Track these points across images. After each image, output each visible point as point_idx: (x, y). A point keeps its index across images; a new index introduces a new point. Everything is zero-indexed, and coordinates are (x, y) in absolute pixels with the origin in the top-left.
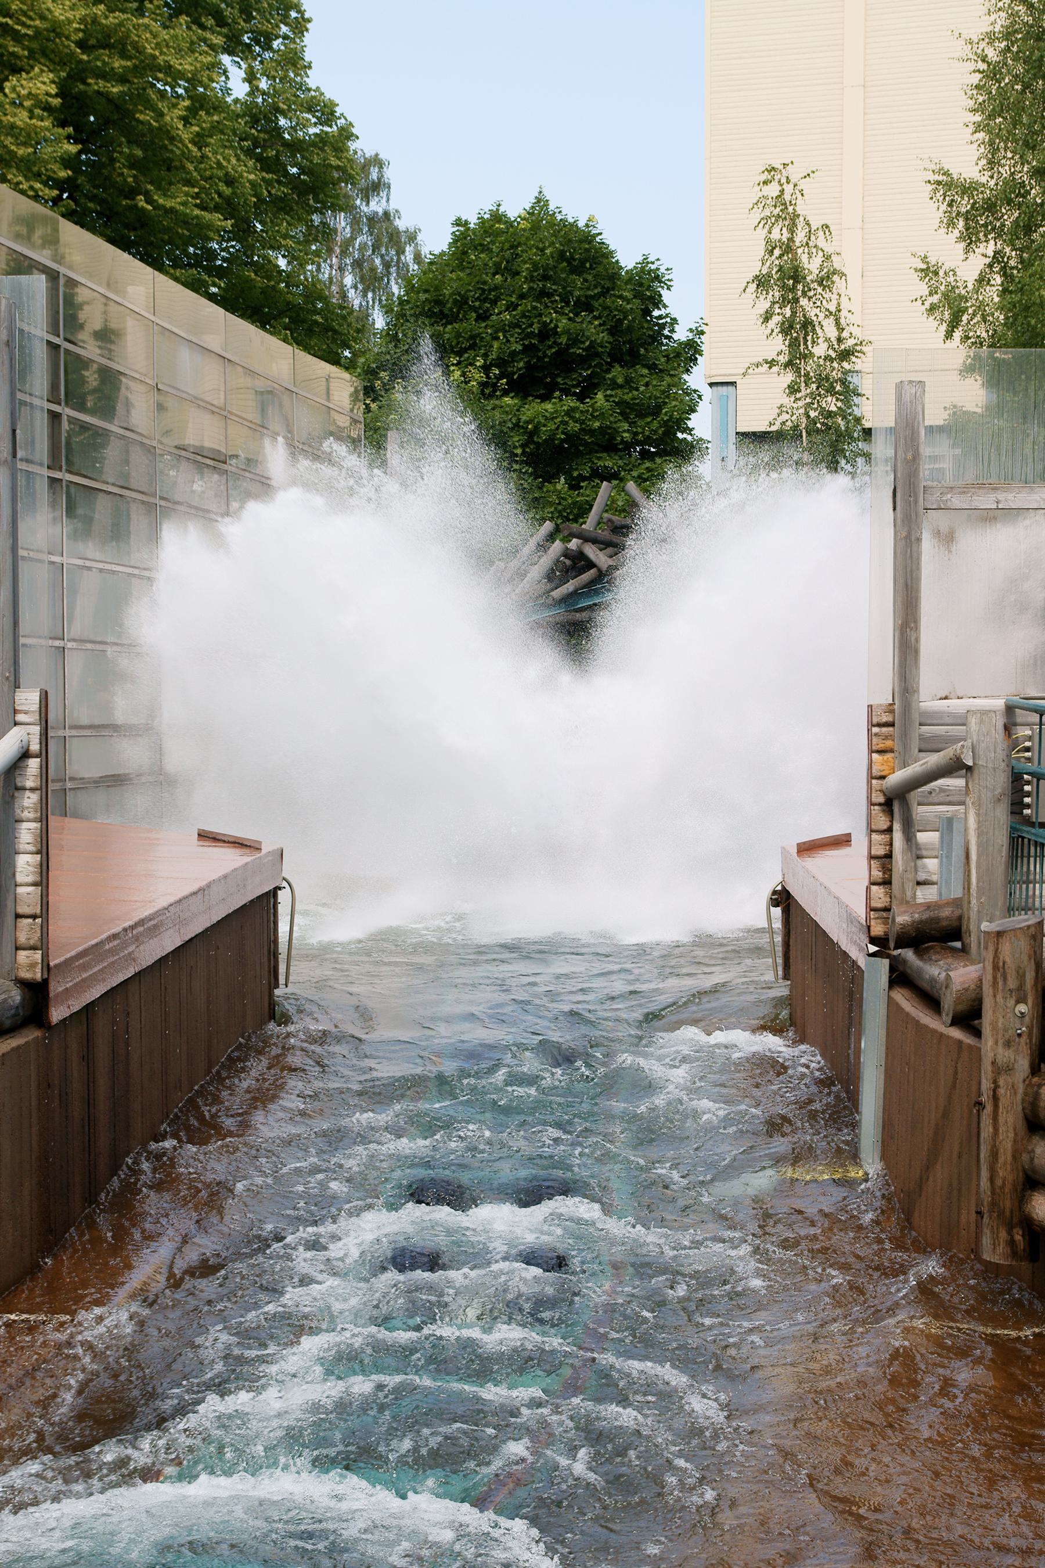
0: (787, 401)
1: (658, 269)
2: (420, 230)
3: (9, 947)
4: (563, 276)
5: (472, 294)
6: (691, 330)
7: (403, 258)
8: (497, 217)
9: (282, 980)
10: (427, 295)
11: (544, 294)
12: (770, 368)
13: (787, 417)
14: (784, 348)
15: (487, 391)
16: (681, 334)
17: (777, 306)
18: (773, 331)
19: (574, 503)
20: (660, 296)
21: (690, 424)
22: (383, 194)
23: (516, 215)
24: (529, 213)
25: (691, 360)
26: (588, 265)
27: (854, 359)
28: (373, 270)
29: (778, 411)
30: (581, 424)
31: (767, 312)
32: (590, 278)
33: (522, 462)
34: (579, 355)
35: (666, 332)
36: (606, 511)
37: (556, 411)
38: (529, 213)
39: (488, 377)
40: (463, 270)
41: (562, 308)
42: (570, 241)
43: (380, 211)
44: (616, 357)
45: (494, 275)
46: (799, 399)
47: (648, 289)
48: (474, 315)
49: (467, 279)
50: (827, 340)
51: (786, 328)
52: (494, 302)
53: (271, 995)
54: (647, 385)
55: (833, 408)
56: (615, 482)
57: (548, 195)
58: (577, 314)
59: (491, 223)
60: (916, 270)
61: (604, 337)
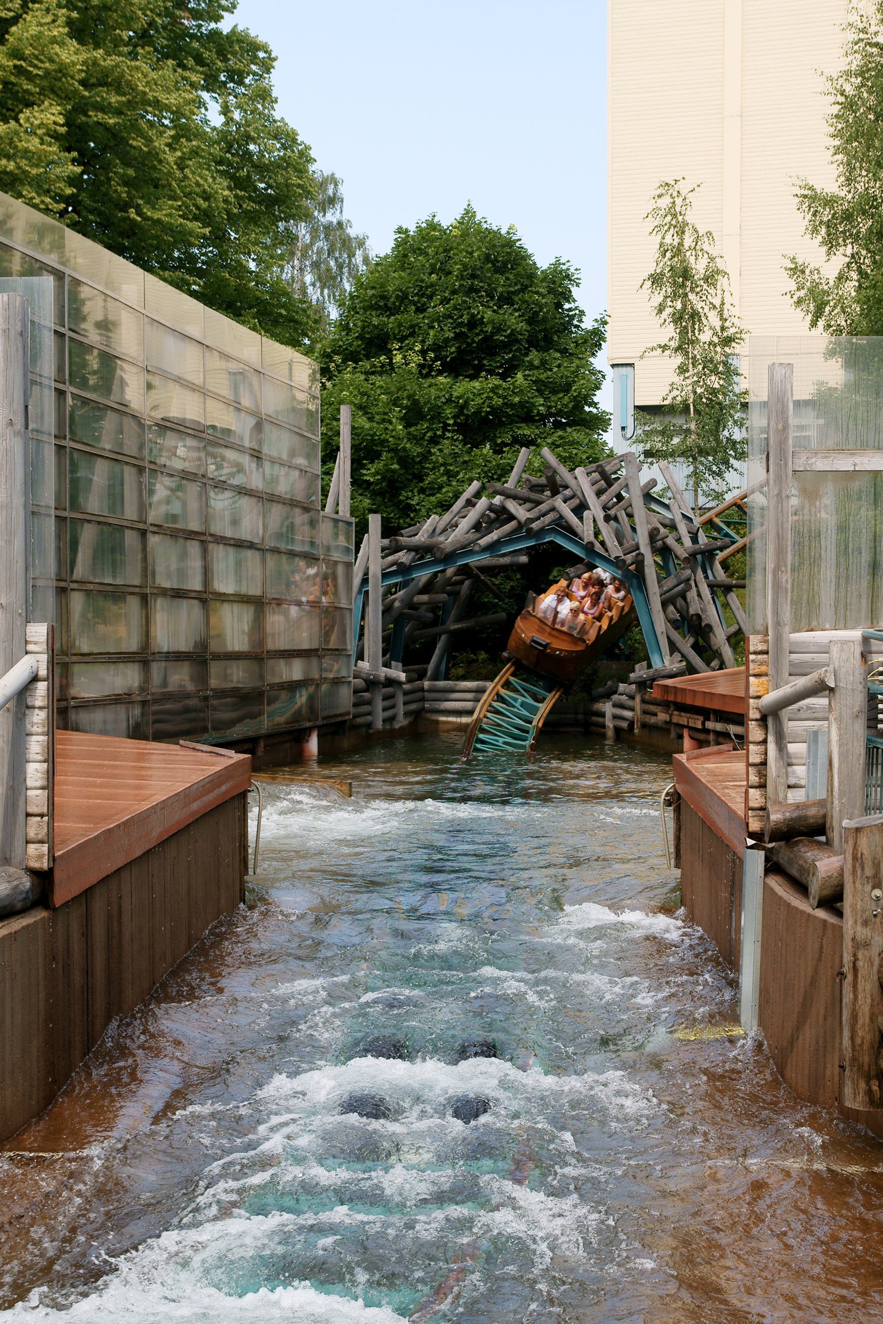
0: (678, 379)
6: (596, 320)
8: (433, 226)
10: (373, 292)
11: (472, 290)
13: (678, 393)
14: (674, 335)
15: (424, 372)
16: (588, 324)
17: (669, 300)
19: (498, 465)
20: (570, 291)
21: (595, 399)
22: (338, 206)
27: (734, 344)
28: (329, 270)
32: (511, 277)
33: (453, 431)
35: (575, 322)
36: (524, 471)
39: (425, 360)
42: (494, 246)
43: (335, 221)
44: (533, 343)
45: (430, 274)
48: (413, 308)
51: (677, 318)
52: (430, 297)
53: (242, 883)
54: (559, 366)
55: (716, 386)
56: (532, 448)
57: (475, 207)
58: (500, 307)
60: (786, 269)
61: (523, 326)
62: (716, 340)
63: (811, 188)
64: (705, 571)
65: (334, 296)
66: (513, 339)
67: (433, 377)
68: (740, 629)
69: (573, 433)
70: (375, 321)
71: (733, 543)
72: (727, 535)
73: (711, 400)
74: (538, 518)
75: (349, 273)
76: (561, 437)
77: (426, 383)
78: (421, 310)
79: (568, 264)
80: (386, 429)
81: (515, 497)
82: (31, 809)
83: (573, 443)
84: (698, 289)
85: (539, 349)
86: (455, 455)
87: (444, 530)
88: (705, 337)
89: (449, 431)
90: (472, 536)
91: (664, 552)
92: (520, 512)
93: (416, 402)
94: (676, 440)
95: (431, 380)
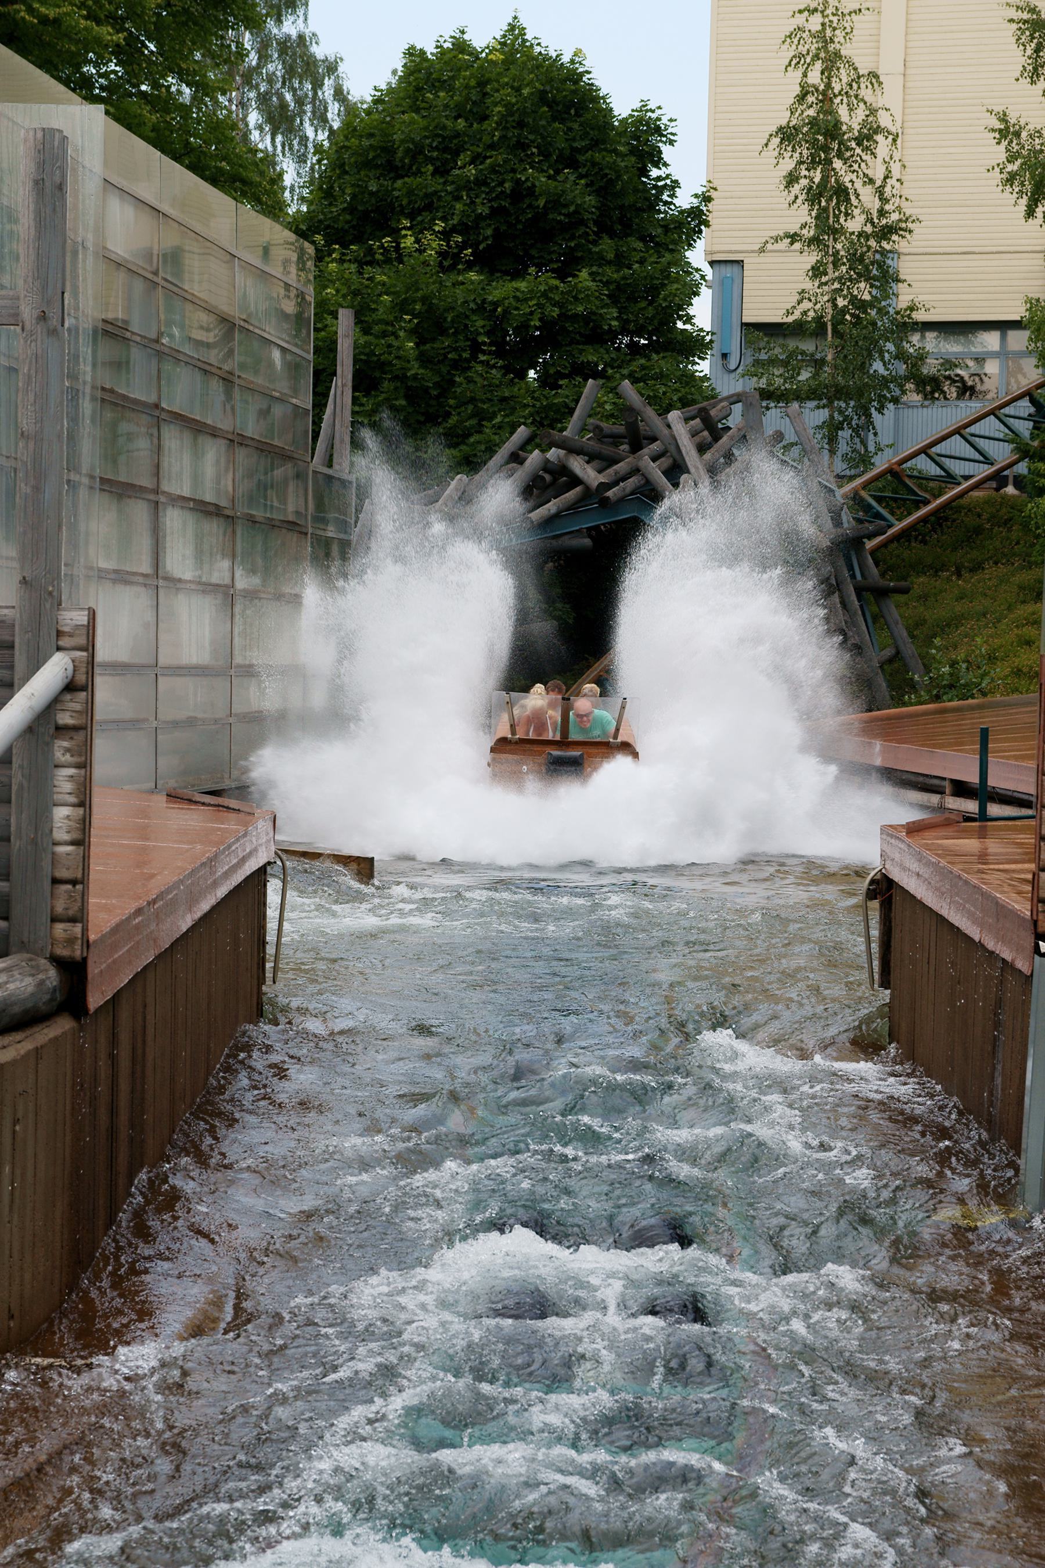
0: (809, 285)
1: (659, 119)
2: (341, 59)
3: (46, 918)
4: (543, 123)
5: (428, 141)
6: (696, 196)
7: (320, 93)
8: (461, 46)
9: (269, 975)
10: (372, 141)
11: (522, 146)
12: (792, 243)
13: (810, 305)
14: (808, 219)
15: (446, 263)
16: (684, 200)
17: (803, 167)
18: (796, 197)
19: (550, 406)
20: (660, 152)
21: (691, 311)
22: (301, 12)
23: (484, 45)
24: (500, 43)
25: (695, 232)
26: (573, 112)
27: (895, 237)
28: (283, 105)
29: (798, 297)
30: (560, 307)
31: (790, 174)
32: (576, 126)
33: (490, 353)
34: (560, 222)
35: (665, 197)
36: (590, 416)
37: (531, 291)
38: (500, 43)
39: (448, 245)
40: (417, 110)
41: (540, 162)
42: (552, 80)
43: (294, 34)
44: (604, 228)
45: (456, 118)
46: (826, 284)
47: (646, 144)
48: (431, 168)
49: (423, 123)
50: (867, 212)
51: (814, 196)
52: (457, 153)
53: (260, 994)
54: (642, 262)
55: (867, 297)
56: (601, 382)
57: (524, 21)
58: (558, 172)
59: (454, 53)
60: (993, 130)
61: (590, 200)
62: (869, 229)
63: (1033, 10)
65: (291, 149)
66: (576, 220)
67: (459, 273)
68: (898, 652)
69: (661, 362)
70: (373, 187)
71: (890, 526)
72: (878, 516)
73: (858, 317)
74: (616, 483)
75: (314, 112)
76: (643, 368)
77: (448, 279)
78: (442, 171)
79: (658, 112)
80: (390, 346)
81: (578, 452)
82: (63, 873)
83: (661, 376)
84: (848, 154)
85: (612, 235)
86: (491, 387)
88: (855, 224)
89: (484, 352)
92: (590, 474)
93: (431, 309)
94: (805, 375)
95: (453, 277)
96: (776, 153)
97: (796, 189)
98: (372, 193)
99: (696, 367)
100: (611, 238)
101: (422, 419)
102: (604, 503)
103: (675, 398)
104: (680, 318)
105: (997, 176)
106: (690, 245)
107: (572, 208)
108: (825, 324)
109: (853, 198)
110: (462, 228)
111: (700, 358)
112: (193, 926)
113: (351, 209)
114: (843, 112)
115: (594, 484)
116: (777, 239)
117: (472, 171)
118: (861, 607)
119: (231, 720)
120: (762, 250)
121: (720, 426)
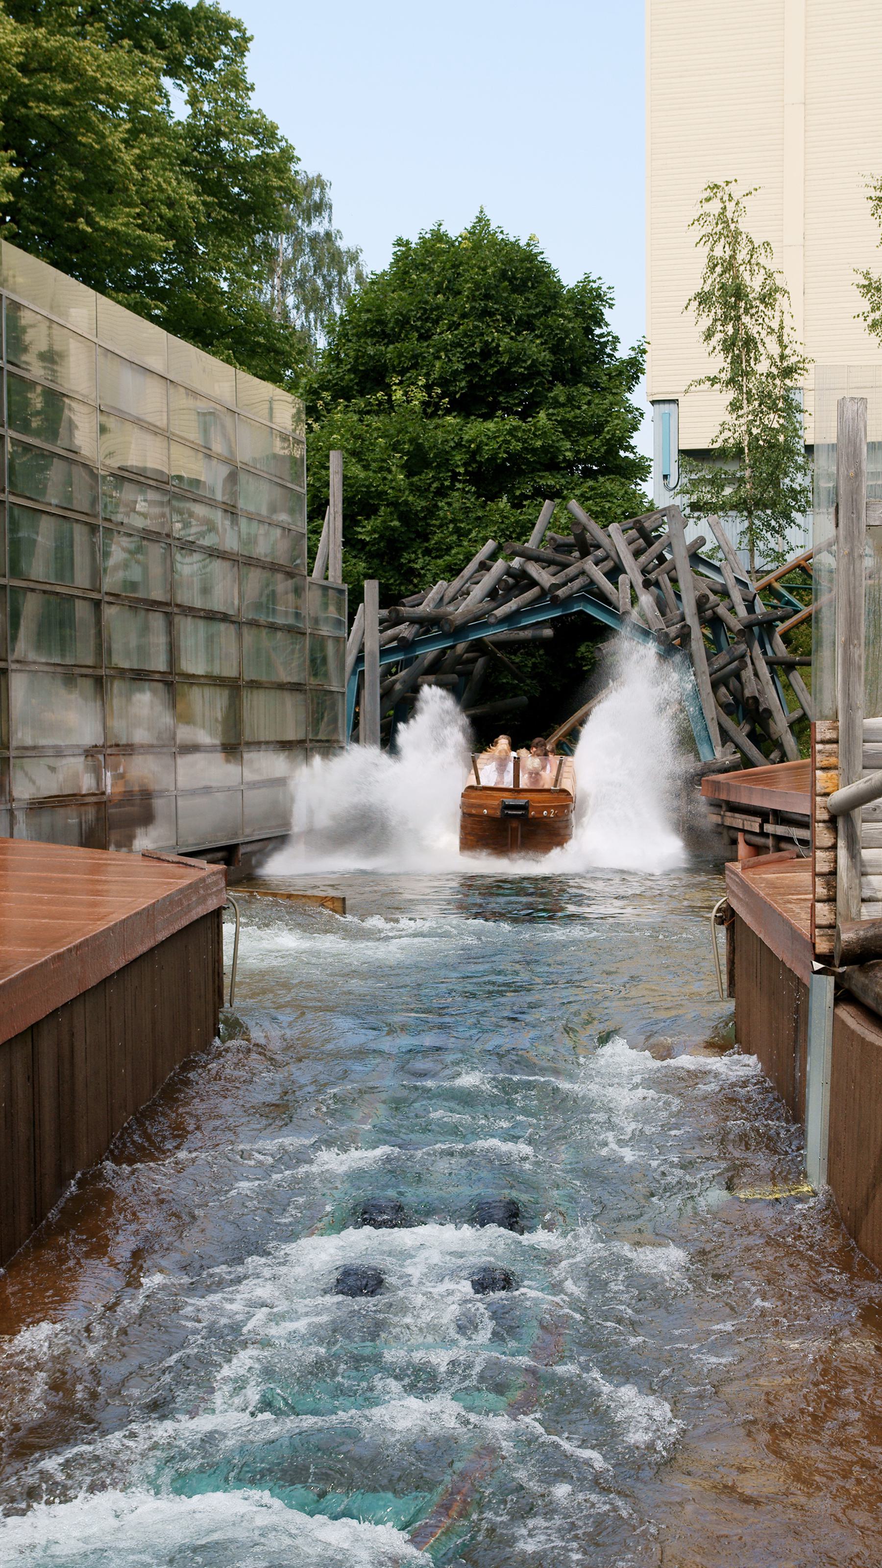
0: (730, 419)
4: (505, 295)
6: (633, 349)
7: (344, 278)
8: (438, 236)
10: (369, 315)
11: (486, 313)
12: (712, 385)
13: (730, 434)
14: (726, 365)
15: (429, 411)
16: (623, 353)
17: (719, 323)
19: (517, 522)
20: (602, 314)
21: (632, 442)
22: (325, 214)
24: (470, 233)
25: (633, 378)
26: (530, 284)
27: (796, 376)
28: (315, 290)
29: (720, 428)
30: (523, 443)
32: (532, 297)
33: (464, 482)
35: (608, 351)
36: (549, 529)
37: (499, 430)
38: (470, 233)
39: (430, 396)
41: (504, 327)
43: (322, 232)
44: (559, 376)
45: (436, 294)
46: (742, 416)
48: (416, 334)
50: (770, 357)
51: (728, 345)
52: (436, 322)
54: (589, 403)
55: (776, 425)
56: (558, 501)
57: (489, 214)
58: (518, 333)
61: (545, 355)
64: (763, 646)
66: (534, 372)
68: (805, 714)
69: (607, 484)
70: (371, 351)
72: (788, 603)
74: (564, 584)
75: (340, 294)
76: (592, 488)
77: (431, 424)
78: (425, 337)
81: (537, 559)
83: (606, 496)
86: (466, 510)
87: (454, 599)
88: (763, 367)
89: (460, 481)
90: (486, 605)
91: (714, 623)
92: (544, 576)
93: (419, 447)
94: (728, 491)
95: (437, 421)
96: (696, 314)
97: (714, 341)
98: (370, 356)
99: (639, 487)
100: (564, 385)
101: (413, 536)
102: (555, 598)
103: (619, 512)
104: (621, 448)
105: (863, 325)
106: (630, 389)
107: (529, 362)
108: (743, 448)
109: (760, 346)
110: (443, 382)
111: (641, 479)
112: (127, 966)
113: (353, 370)
114: (746, 276)
115: (547, 585)
116: (700, 382)
117: (448, 336)
118: (772, 678)
119: (242, 787)
120: (686, 392)
121: (653, 534)
